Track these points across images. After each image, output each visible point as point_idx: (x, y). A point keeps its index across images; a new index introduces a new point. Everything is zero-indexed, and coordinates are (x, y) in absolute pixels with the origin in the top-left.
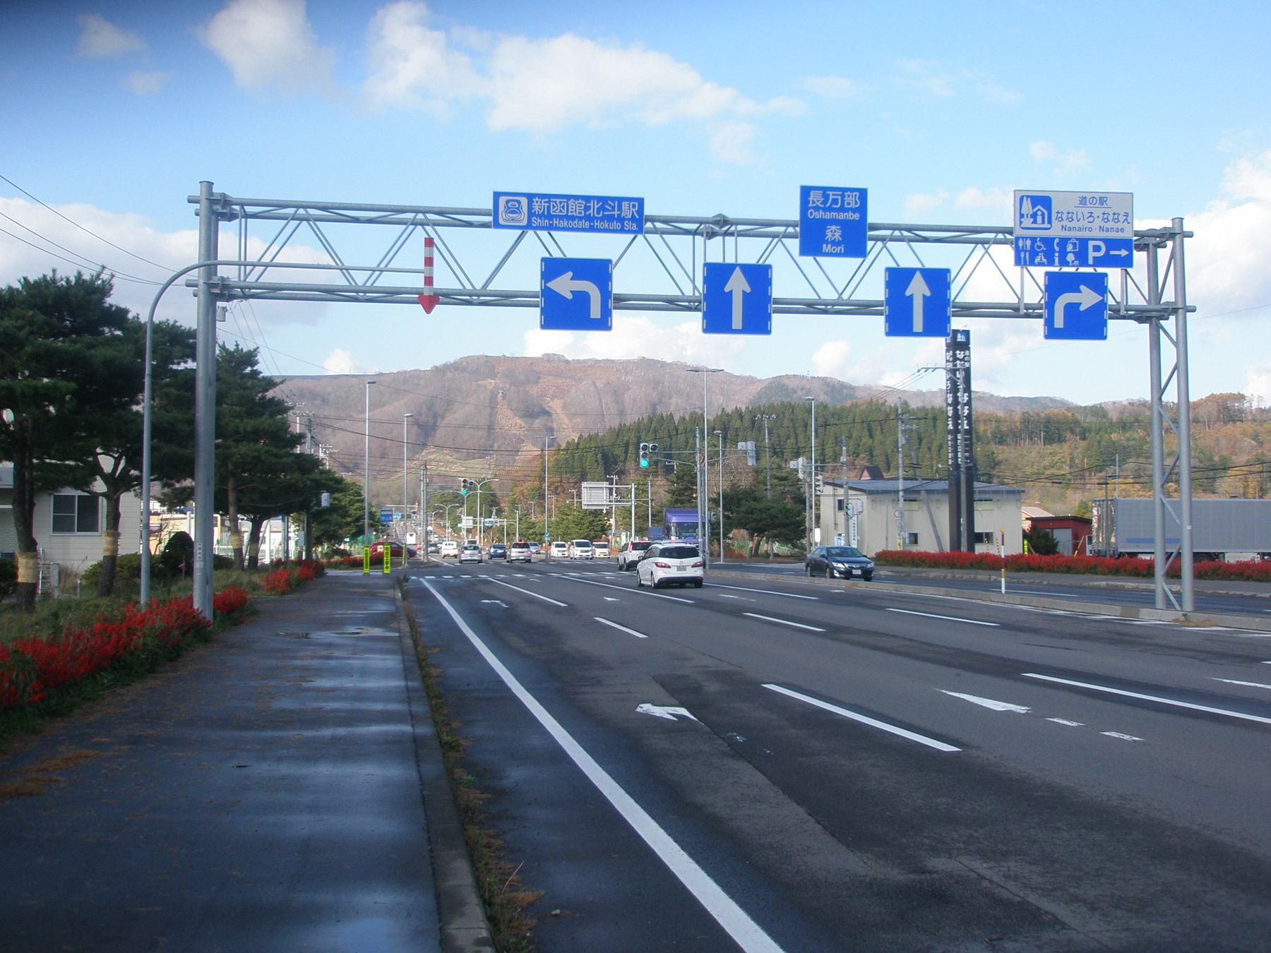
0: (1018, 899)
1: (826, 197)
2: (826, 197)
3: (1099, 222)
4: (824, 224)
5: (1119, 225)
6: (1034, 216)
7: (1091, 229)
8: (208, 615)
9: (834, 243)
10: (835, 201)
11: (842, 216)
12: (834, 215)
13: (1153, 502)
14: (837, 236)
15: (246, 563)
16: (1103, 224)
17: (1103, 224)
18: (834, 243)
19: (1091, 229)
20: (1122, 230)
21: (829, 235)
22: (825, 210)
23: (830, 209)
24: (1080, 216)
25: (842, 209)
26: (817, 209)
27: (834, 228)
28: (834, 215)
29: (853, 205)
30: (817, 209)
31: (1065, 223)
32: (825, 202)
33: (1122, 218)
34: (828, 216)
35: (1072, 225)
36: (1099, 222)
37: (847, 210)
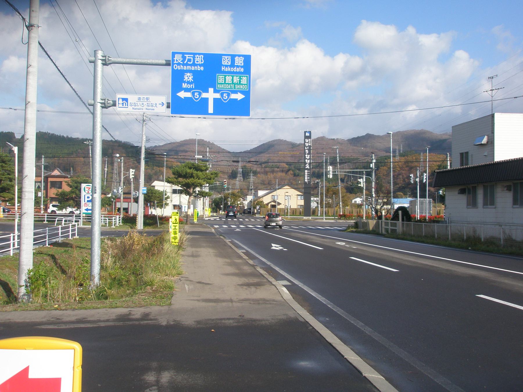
0: (303, 320)
1: (184, 58)
2: (184, 58)
3: (145, 107)
4: (183, 72)
5: (153, 108)
6: (123, 104)
7: (142, 109)
8: (153, 184)
9: (188, 83)
10: (189, 60)
11: (193, 68)
12: (189, 67)
13: (391, 223)
14: (191, 79)
15: (72, 169)
16: (147, 107)
17: (147, 107)
18: (188, 83)
19: (142, 109)
20: (154, 109)
21: (186, 78)
22: (184, 65)
23: (187, 65)
24: (139, 104)
25: (194, 64)
26: (179, 64)
27: (189, 74)
28: (189, 67)
29: (200, 62)
30: (179, 64)
31: (133, 107)
32: (183, 61)
33: (154, 105)
34: (185, 68)
35: (136, 107)
36: (145, 107)
37: (197, 65)
